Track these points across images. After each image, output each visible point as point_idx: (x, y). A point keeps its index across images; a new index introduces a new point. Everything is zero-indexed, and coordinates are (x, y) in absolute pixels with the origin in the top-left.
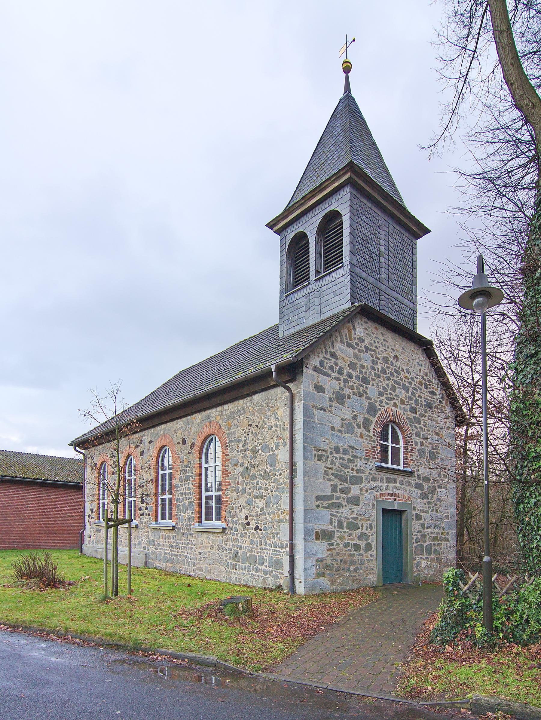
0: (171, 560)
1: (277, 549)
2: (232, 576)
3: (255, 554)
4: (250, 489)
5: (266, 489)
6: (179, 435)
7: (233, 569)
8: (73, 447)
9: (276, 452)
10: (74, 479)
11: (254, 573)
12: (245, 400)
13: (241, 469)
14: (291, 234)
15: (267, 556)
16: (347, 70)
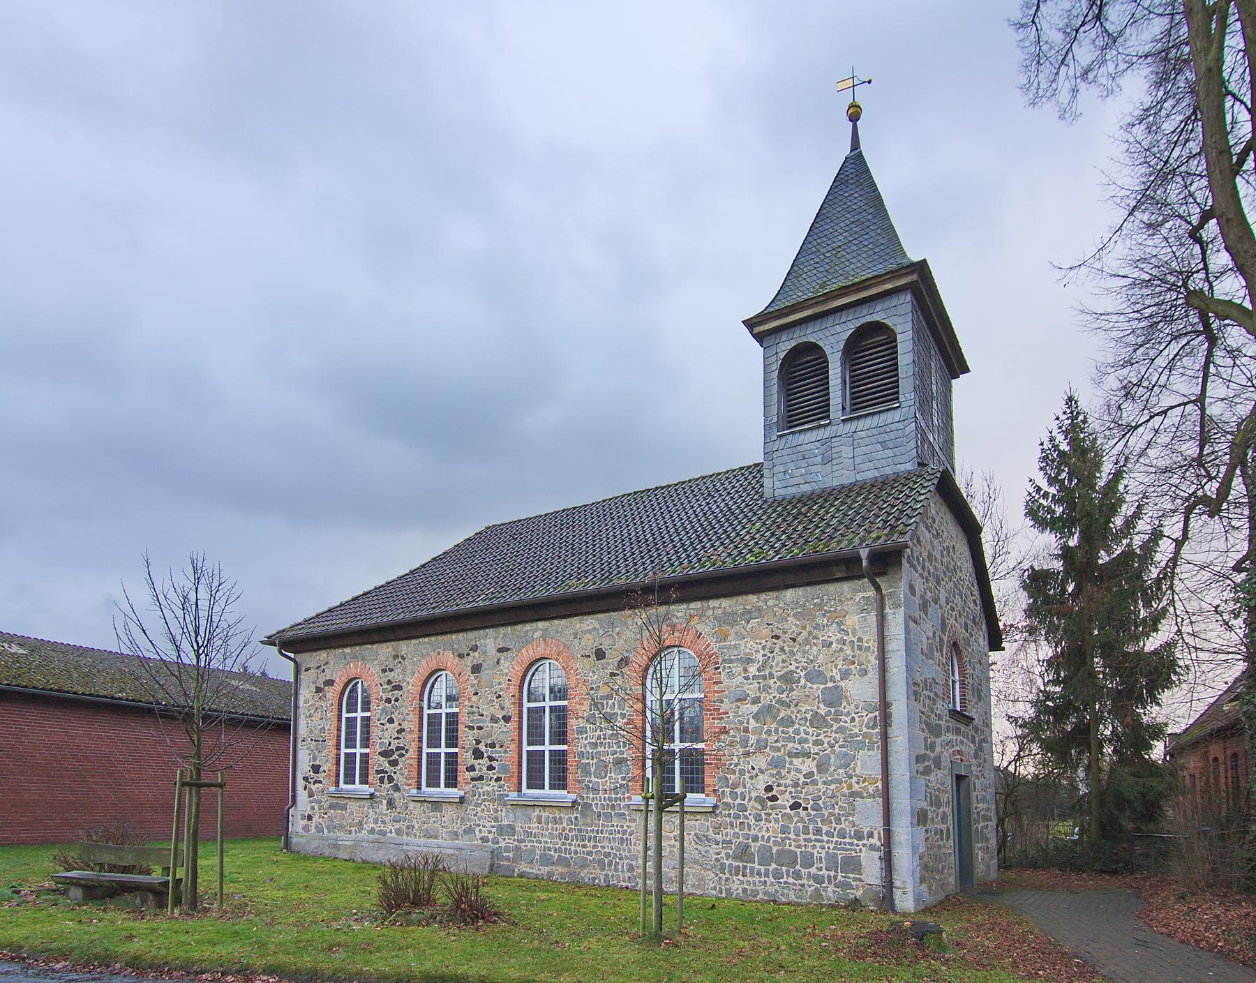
0: (563, 861)
1: (847, 840)
2: (734, 886)
3: (793, 848)
4: (777, 741)
5: (816, 743)
6: (590, 642)
7: (737, 874)
8: (276, 648)
9: (842, 684)
10: (272, 708)
11: (791, 880)
12: (763, 596)
13: (755, 708)
14: (786, 344)
15: (824, 852)
16: (854, 117)
